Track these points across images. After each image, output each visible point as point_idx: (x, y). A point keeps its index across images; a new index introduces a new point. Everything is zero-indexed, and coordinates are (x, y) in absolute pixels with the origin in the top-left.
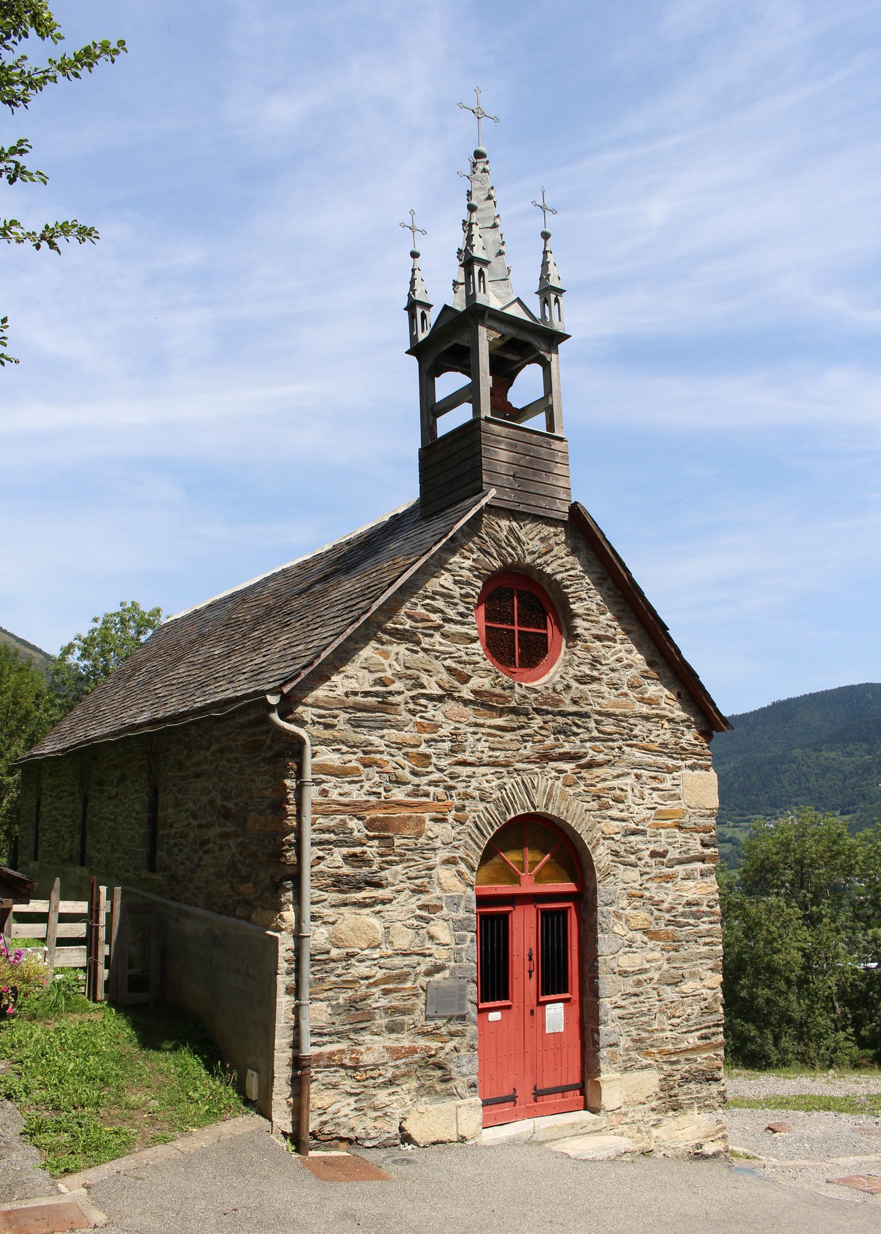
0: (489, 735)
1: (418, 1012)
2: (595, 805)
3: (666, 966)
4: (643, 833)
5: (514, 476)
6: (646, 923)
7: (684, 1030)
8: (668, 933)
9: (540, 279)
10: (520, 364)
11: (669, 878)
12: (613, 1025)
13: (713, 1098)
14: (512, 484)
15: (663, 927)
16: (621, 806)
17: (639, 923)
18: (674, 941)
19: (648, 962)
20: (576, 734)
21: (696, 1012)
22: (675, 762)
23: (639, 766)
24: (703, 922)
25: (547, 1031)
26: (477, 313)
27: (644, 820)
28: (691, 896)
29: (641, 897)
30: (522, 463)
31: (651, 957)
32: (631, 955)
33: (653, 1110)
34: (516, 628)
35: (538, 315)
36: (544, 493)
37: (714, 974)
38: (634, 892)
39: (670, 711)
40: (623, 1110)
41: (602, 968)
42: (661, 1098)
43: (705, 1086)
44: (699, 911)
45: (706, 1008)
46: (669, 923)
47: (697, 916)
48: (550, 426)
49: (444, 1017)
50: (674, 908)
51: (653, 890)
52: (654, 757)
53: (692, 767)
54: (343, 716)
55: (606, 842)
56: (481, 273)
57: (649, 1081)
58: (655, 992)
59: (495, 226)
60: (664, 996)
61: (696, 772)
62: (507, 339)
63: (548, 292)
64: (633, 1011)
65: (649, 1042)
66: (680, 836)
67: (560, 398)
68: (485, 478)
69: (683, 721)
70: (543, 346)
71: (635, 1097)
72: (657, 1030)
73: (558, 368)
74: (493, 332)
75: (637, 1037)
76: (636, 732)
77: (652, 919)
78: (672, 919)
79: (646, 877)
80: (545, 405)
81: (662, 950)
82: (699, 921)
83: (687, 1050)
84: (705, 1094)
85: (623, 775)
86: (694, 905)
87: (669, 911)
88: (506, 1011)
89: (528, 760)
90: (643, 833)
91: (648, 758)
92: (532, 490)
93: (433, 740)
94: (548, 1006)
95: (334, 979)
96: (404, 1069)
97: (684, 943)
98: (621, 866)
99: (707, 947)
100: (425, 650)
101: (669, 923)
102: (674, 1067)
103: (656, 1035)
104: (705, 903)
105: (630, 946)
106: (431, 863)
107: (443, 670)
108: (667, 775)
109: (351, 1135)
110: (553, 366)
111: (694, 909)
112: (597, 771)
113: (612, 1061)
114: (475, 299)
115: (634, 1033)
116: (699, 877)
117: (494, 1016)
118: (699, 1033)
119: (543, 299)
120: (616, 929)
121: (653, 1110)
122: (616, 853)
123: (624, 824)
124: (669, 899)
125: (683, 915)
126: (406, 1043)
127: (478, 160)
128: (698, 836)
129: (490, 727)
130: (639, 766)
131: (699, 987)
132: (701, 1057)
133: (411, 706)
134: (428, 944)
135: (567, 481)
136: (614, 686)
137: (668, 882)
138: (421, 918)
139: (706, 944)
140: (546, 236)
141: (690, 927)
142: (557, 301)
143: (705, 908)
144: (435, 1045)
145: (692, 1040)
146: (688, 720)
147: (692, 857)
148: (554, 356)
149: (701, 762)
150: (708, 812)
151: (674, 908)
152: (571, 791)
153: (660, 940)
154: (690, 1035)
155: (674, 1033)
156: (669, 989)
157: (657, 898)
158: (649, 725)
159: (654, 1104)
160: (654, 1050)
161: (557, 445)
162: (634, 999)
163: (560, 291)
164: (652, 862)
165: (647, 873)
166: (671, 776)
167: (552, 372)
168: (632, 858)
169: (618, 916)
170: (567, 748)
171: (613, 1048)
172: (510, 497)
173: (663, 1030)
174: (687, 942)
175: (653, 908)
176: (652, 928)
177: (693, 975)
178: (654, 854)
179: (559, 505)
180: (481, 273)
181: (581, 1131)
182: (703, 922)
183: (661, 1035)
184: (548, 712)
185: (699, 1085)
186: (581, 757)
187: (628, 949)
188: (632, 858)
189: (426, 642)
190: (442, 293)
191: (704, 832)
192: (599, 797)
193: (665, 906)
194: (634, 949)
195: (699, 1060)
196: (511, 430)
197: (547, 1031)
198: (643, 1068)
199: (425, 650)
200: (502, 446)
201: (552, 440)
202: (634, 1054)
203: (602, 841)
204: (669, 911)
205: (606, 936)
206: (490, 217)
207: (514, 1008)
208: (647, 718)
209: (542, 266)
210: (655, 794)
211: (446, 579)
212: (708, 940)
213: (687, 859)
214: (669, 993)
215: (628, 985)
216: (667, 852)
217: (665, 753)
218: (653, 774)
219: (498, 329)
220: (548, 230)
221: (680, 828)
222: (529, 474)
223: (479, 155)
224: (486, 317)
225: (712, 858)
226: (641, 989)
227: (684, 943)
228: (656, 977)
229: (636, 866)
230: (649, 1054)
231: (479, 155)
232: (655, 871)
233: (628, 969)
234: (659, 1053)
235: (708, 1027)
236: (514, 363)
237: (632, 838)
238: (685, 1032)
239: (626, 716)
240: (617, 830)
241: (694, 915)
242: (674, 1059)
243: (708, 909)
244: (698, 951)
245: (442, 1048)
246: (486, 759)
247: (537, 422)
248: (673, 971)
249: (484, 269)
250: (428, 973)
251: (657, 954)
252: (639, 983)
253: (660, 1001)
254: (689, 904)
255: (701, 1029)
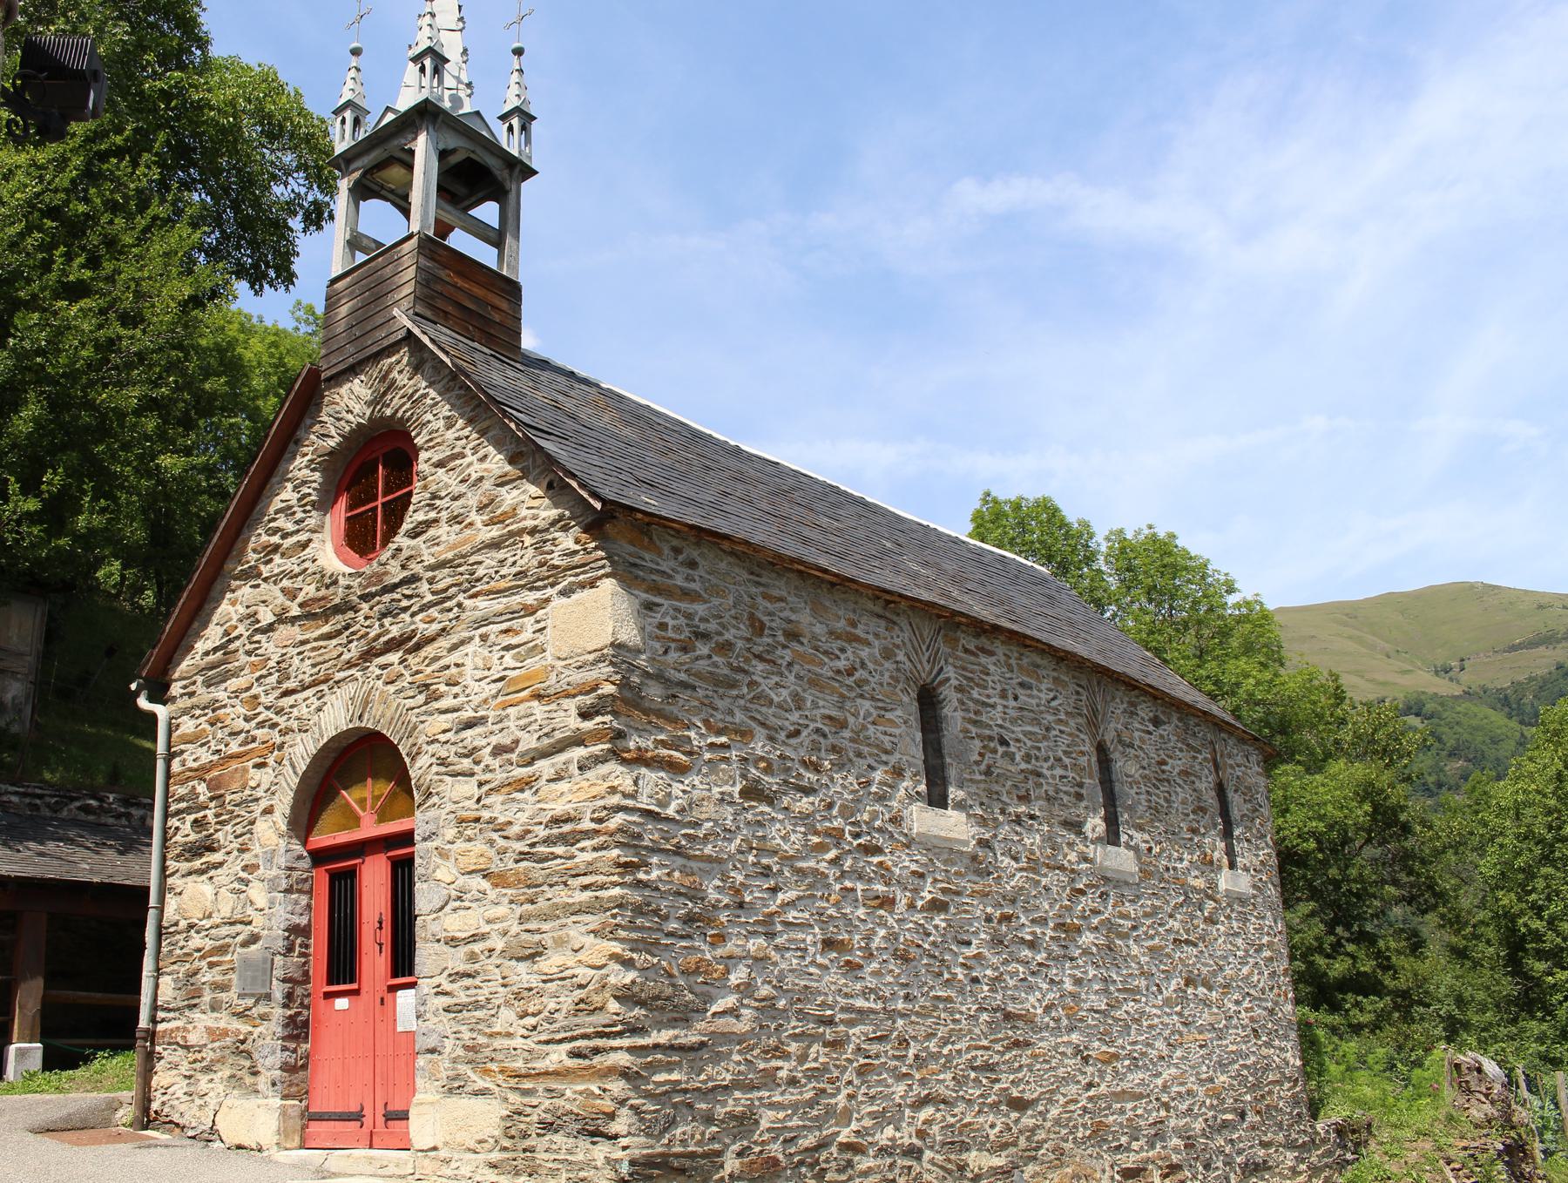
0: (314, 649)
1: (234, 989)
2: (421, 698)
3: (515, 929)
4: (482, 721)
6: (482, 860)
7: (544, 1037)
8: (528, 868)
11: (524, 784)
12: (436, 1020)
13: (596, 1168)
15: (511, 865)
16: (456, 689)
17: (470, 862)
18: (529, 887)
19: (488, 922)
20: (405, 609)
21: (565, 1008)
22: (538, 595)
23: (485, 621)
24: (582, 850)
25: (399, 1029)
27: (485, 701)
28: (559, 808)
29: (477, 820)
31: (493, 914)
32: (462, 912)
33: (493, 1166)
34: (381, 500)
37: (599, 941)
38: (465, 814)
39: (535, 517)
40: (443, 1154)
41: (419, 932)
42: (505, 1149)
43: (584, 1143)
44: (573, 831)
45: (582, 1001)
46: (523, 856)
47: (569, 840)
49: (252, 995)
50: (529, 832)
51: (498, 807)
52: (504, 600)
53: (565, 593)
54: (200, 679)
55: (431, 749)
57: (486, 1116)
58: (497, 971)
60: (512, 979)
61: (574, 597)
64: (465, 1000)
65: (487, 1052)
66: (538, 709)
69: (553, 524)
71: (461, 1137)
72: (499, 1033)
75: (470, 1043)
76: (481, 572)
77: (492, 853)
78: (527, 849)
79: (486, 788)
81: (511, 902)
82: (573, 849)
83: (547, 1073)
84: (580, 1157)
85: (462, 643)
86: (566, 821)
87: (520, 838)
88: (354, 998)
89: (350, 665)
90: (482, 721)
91: (499, 604)
93: (262, 677)
94: (400, 993)
95: (178, 952)
96: (219, 1053)
97: (545, 888)
98: (446, 778)
99: (588, 894)
100: (265, 580)
101: (523, 856)
102: (526, 1100)
103: (498, 1043)
104: (588, 815)
105: (459, 898)
106: (254, 815)
107: (279, 594)
108: (526, 620)
109: (180, 1121)
111: (567, 828)
112: (429, 651)
113: (433, 1077)
115: (467, 1035)
116: (577, 772)
117: (342, 1003)
118: (567, 1046)
120: (439, 875)
121: (493, 1166)
122: (443, 762)
123: (455, 715)
124: (523, 817)
125: (547, 841)
126: (222, 1024)
128: (571, 705)
129: (316, 640)
130: (485, 621)
131: (570, 964)
132: (571, 1089)
133: (248, 647)
134: (250, 911)
136: (455, 519)
137: (522, 791)
138: (241, 880)
139: (585, 888)
141: (559, 861)
143: (587, 825)
144: (245, 1028)
145: (558, 1056)
146: (561, 518)
147: (560, 741)
149: (581, 577)
150: (591, 657)
151: (529, 832)
152: (391, 689)
153: (508, 886)
154: (555, 1047)
155: (528, 1041)
156: (522, 967)
157: (502, 819)
158: (501, 555)
159: (496, 1156)
160: (494, 1066)
162: (468, 982)
164: (495, 763)
165: (487, 782)
166: (532, 619)
168: (466, 763)
169: (444, 855)
170: (395, 631)
171: (435, 1056)
173: (509, 1035)
174: (551, 886)
175: (495, 836)
176: (494, 869)
177: (560, 943)
178: (499, 750)
181: (380, 1172)
182: (582, 850)
183: (507, 1042)
184: (373, 595)
185: (572, 1140)
186: (410, 638)
187: (458, 904)
188: (466, 763)
189: (265, 570)
191: (581, 693)
192: (427, 686)
193: (515, 830)
194: (467, 904)
195: (568, 1093)
197: (399, 1029)
198: (476, 1093)
199: (265, 580)
202: (464, 1069)
203: (425, 747)
204: (520, 838)
205: (425, 886)
207: (363, 991)
208: (495, 545)
210: (508, 656)
211: (288, 494)
212: (587, 880)
213: (552, 746)
214: (523, 974)
215: (456, 960)
216: (517, 742)
217: (522, 587)
218: (504, 626)
221: (538, 697)
225: (596, 736)
226: (477, 966)
227: (545, 888)
228: (499, 944)
229: (472, 775)
230: (487, 1072)
232: (499, 777)
233: (458, 935)
234: (502, 1072)
235: (585, 1036)
237: (468, 733)
238: (547, 1042)
239: (463, 556)
240: (446, 726)
241: (564, 839)
242: (528, 1085)
243: (594, 826)
244: (570, 901)
245: (251, 1033)
246: (308, 680)
248: (525, 936)
250: (245, 944)
251: (502, 910)
252: (473, 958)
253: (504, 986)
254: (556, 821)
255: (573, 1039)
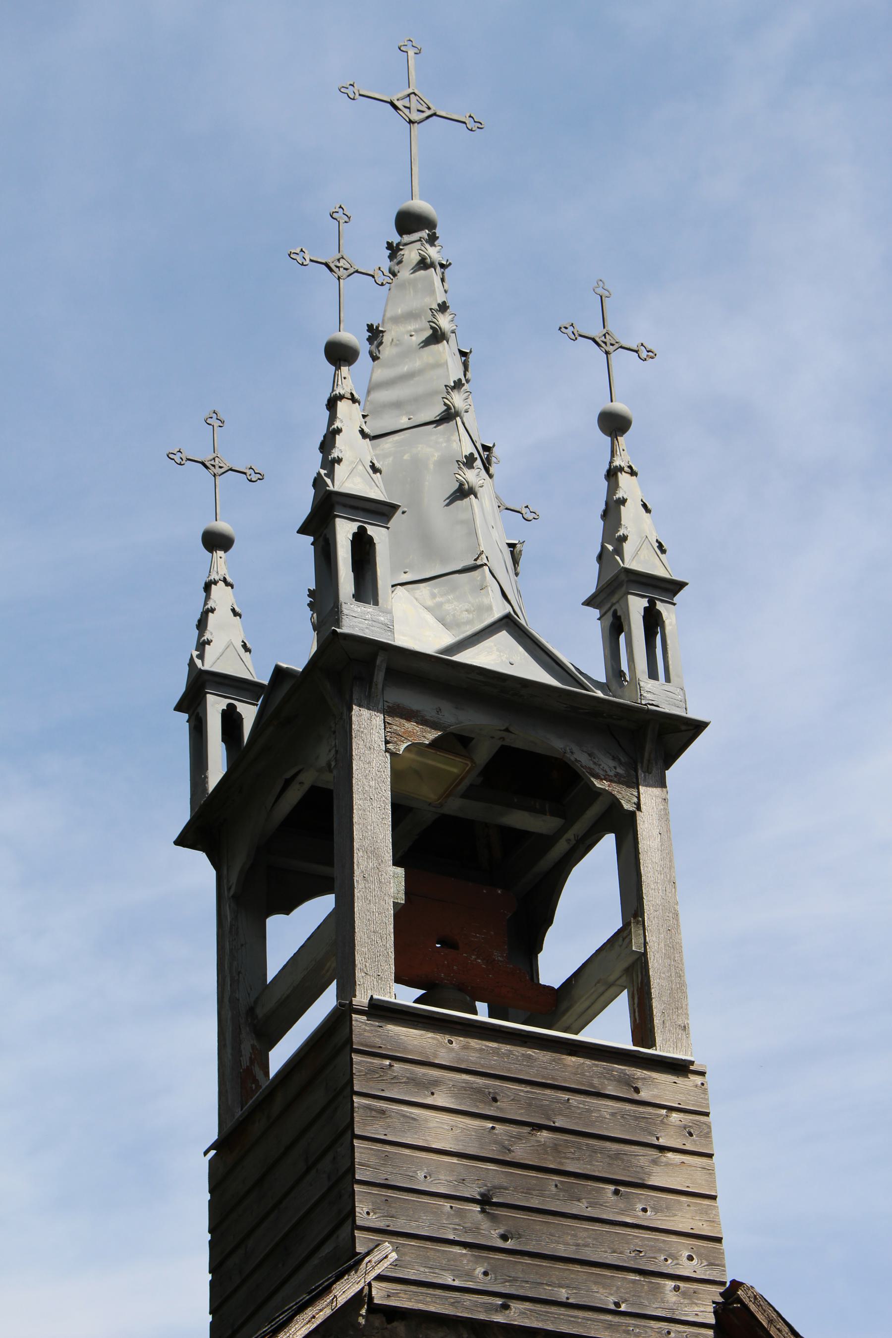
5: (485, 1201)
9: (600, 558)
10: (561, 847)
14: (476, 1230)
26: (350, 669)
30: (520, 1153)
35: (595, 668)
36: (611, 1259)
48: (643, 1029)
56: (362, 546)
59: (449, 416)
62: (483, 753)
63: (629, 595)
67: (672, 929)
68: (365, 1211)
70: (608, 764)
73: (666, 833)
74: (410, 726)
80: (623, 965)
92: (562, 1250)
110: (647, 826)
114: (338, 623)
119: (609, 618)
127: (407, 238)
135: (705, 1212)
140: (614, 424)
142: (653, 622)
148: (649, 795)
161: (660, 1087)
163: (671, 588)
167: (643, 845)
172: (469, 1275)
179: (672, 1298)
180: (362, 546)
190: (264, 634)
196: (474, 1043)
200: (440, 1100)
201: (639, 1073)
206: (435, 393)
209: (605, 515)
219: (430, 714)
220: (620, 406)
222: (550, 1194)
223: (409, 222)
224: (379, 677)
231: (409, 222)
236: (548, 841)
247: (611, 1027)
249: (371, 530)
